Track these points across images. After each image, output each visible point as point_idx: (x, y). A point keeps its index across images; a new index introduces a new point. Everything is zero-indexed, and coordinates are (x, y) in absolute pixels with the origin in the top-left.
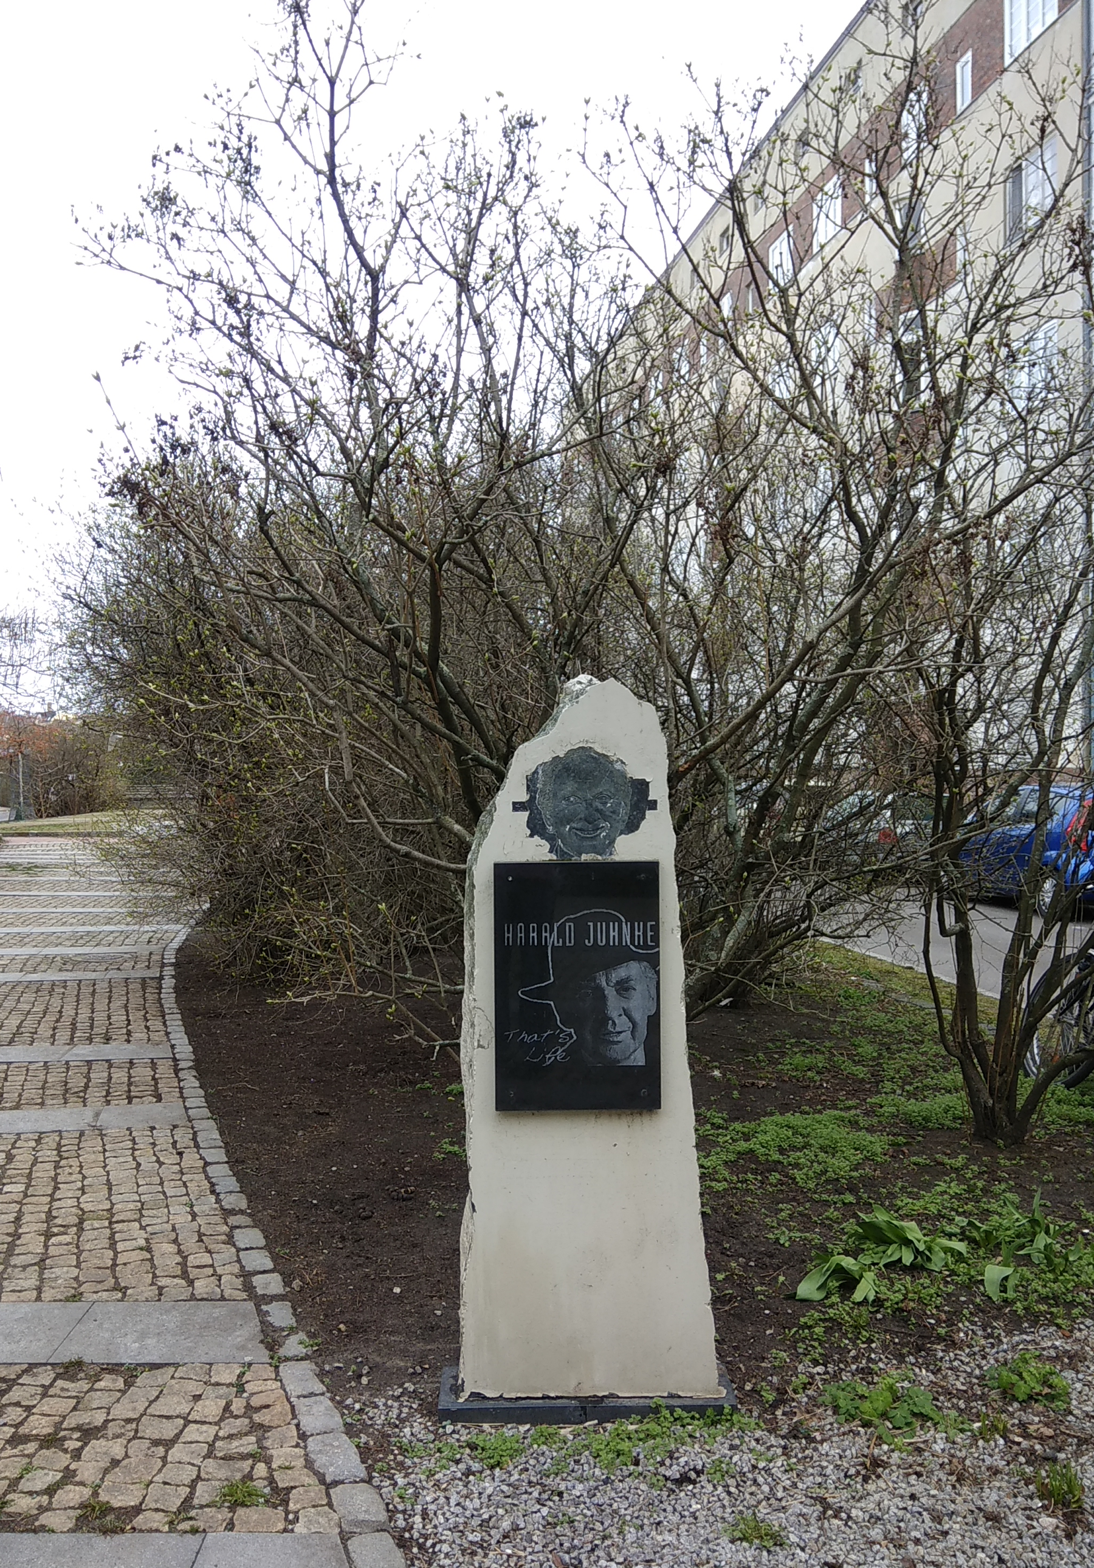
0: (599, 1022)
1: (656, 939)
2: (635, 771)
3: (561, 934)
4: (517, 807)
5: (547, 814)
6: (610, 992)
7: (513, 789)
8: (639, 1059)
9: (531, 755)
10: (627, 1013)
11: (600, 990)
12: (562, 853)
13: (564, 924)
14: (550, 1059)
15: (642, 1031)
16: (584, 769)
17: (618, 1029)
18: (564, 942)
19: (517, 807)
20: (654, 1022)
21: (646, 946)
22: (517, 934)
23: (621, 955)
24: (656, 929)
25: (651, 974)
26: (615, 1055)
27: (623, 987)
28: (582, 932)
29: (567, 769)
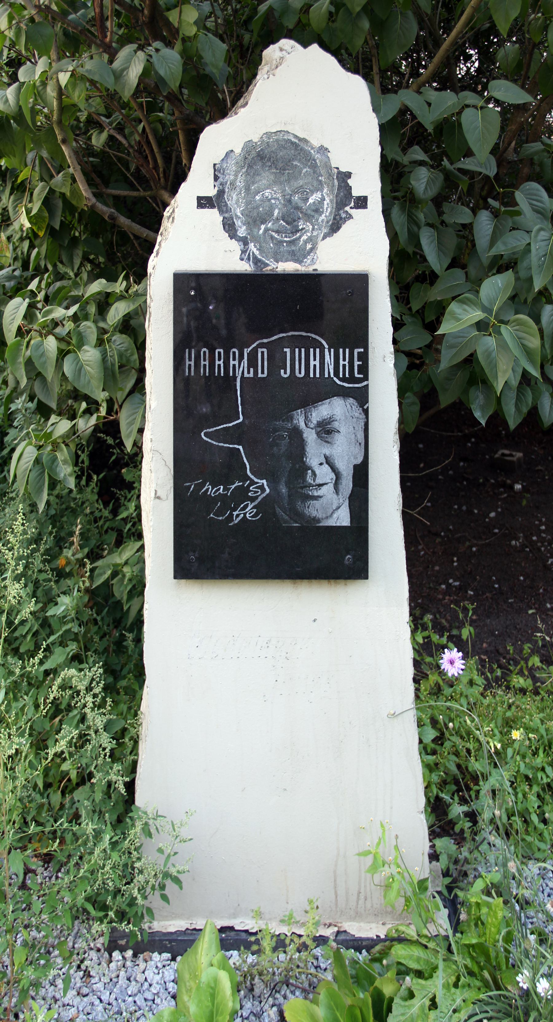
0: (296, 469)
1: (364, 369)
2: (340, 160)
3: (252, 363)
4: (204, 202)
5: (237, 210)
6: (310, 436)
7: (199, 180)
8: (342, 518)
9: (218, 142)
10: (329, 461)
11: (297, 434)
12: (257, 261)
13: (255, 351)
14: (238, 516)
15: (347, 484)
16: (280, 157)
17: (318, 481)
18: (256, 372)
19: (204, 202)
20: (361, 473)
21: (352, 379)
22: (202, 361)
23: (315, 391)
24: (364, 357)
25: (357, 412)
26: (314, 514)
27: (326, 430)
28: (276, 362)
29: (261, 156)
